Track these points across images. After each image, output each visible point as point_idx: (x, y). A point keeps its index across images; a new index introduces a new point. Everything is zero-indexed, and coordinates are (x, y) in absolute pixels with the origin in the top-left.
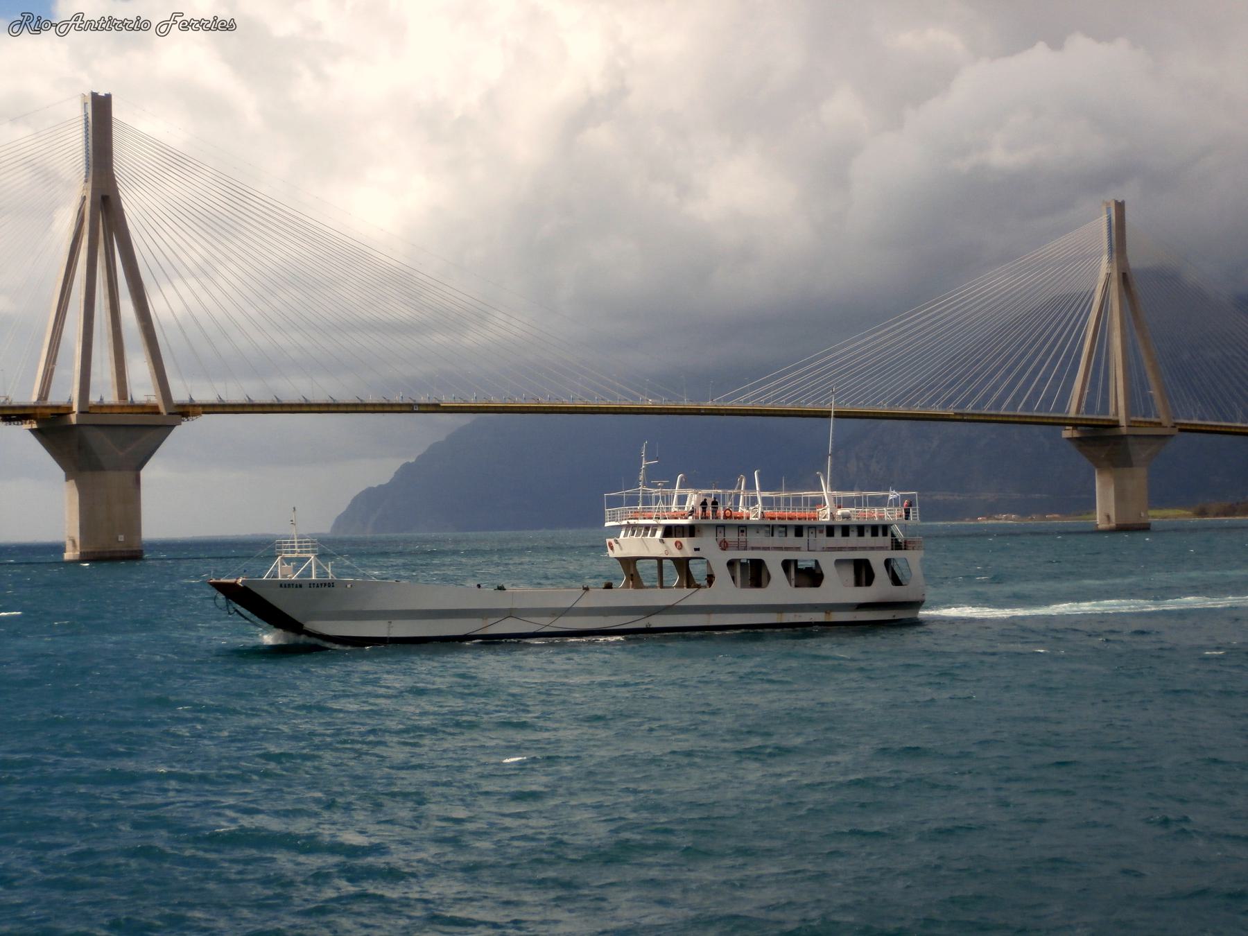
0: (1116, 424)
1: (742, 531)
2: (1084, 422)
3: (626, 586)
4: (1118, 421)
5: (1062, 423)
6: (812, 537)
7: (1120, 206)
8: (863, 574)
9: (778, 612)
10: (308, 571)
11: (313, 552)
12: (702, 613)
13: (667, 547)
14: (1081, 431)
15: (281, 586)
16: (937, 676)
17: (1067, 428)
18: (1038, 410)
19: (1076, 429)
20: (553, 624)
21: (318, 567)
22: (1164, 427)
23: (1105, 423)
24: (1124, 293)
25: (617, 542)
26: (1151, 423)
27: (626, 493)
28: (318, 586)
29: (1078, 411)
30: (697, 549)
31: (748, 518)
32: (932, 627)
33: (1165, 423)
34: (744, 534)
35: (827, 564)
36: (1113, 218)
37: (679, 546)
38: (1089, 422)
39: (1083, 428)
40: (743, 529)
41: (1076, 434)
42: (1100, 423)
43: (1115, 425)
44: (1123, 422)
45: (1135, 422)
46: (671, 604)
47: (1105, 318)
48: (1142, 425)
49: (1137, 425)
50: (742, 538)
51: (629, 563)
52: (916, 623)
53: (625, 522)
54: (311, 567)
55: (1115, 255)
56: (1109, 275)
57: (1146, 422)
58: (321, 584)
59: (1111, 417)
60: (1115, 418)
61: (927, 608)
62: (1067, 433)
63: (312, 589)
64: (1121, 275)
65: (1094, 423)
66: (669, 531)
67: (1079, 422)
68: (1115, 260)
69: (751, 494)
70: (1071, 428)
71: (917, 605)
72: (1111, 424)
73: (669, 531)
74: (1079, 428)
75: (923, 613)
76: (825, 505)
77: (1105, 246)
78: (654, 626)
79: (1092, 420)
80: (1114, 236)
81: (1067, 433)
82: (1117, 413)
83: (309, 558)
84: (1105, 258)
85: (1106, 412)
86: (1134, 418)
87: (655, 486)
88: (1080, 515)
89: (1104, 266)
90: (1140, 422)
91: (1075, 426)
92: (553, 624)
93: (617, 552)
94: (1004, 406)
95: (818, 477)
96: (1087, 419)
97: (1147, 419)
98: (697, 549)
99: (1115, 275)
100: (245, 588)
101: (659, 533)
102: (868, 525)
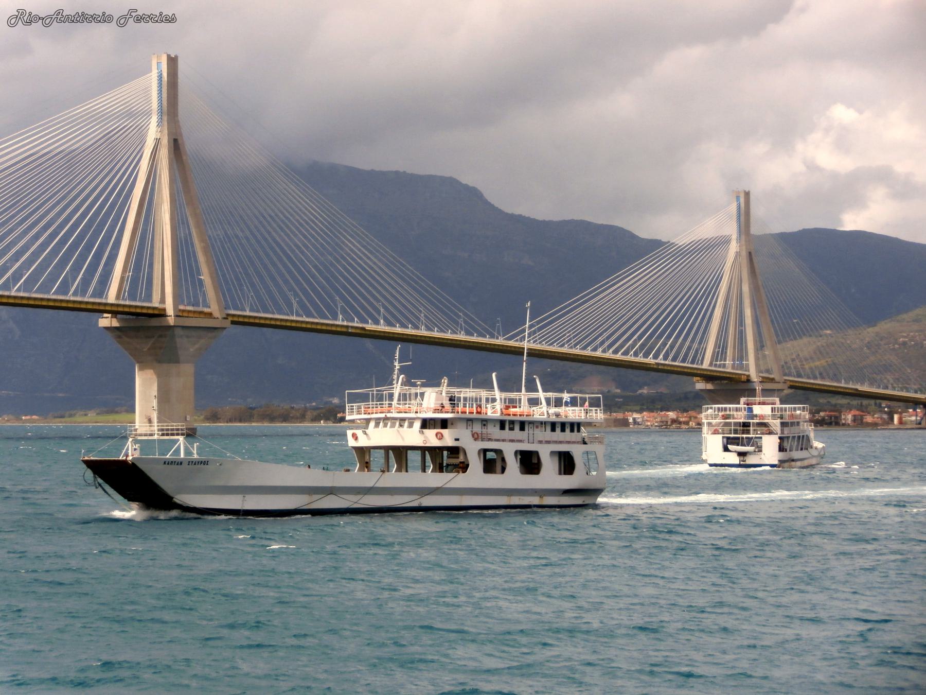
0: (163, 313)
1: (484, 425)
2: (127, 310)
3: (361, 469)
4: (164, 310)
5: (100, 310)
6: (531, 432)
7: (173, 62)
8: (567, 463)
9: (508, 496)
10: (178, 451)
11: (182, 434)
12: (503, 495)
13: (426, 437)
14: (119, 321)
15: (165, 463)
16: (844, 540)
17: (105, 315)
18: (75, 294)
19: (116, 317)
20: (360, 502)
21: (186, 449)
22: (215, 318)
23: (150, 312)
24: (175, 166)
25: (365, 433)
26: (201, 313)
27: (377, 391)
28: (178, 464)
29: (118, 297)
30: (457, 440)
31: (486, 414)
32: (610, 512)
33: (217, 314)
34: (486, 427)
35: (545, 454)
36: (165, 75)
37: (440, 437)
38: (133, 310)
39: (125, 316)
40: (485, 422)
41: (115, 323)
42: (144, 311)
43: (161, 314)
44: (170, 311)
45: (183, 311)
46: (439, 485)
47: (153, 189)
48: (191, 315)
49: (185, 314)
50: (484, 431)
51: (362, 452)
52: (596, 507)
53: (383, 415)
54: (180, 449)
55: (165, 118)
56: (158, 141)
57: (194, 312)
58: (198, 462)
59: (155, 303)
60: (161, 306)
61: (605, 496)
62: (106, 321)
63: (190, 466)
64: (172, 141)
65: (139, 311)
66: (426, 424)
67: (120, 309)
68: (166, 123)
69: (533, 395)
70: (109, 315)
71: (597, 492)
72: (156, 312)
73: (426, 424)
74: (119, 316)
75: (601, 500)
76: (541, 404)
77: (155, 105)
78: (424, 505)
79: (136, 307)
80: (165, 95)
81: (106, 321)
82: (163, 300)
83: (178, 440)
84: (154, 120)
85: (149, 297)
86: (181, 307)
87: (414, 385)
88: (62, 417)
89: (154, 131)
90: (189, 311)
91: (115, 313)
92: (360, 502)
93: (352, 443)
94: (91, 290)
95: (535, 379)
96: (130, 306)
97: (196, 309)
98: (457, 440)
99: (165, 141)
100: (133, 464)
101: (418, 425)
102: (568, 422)
